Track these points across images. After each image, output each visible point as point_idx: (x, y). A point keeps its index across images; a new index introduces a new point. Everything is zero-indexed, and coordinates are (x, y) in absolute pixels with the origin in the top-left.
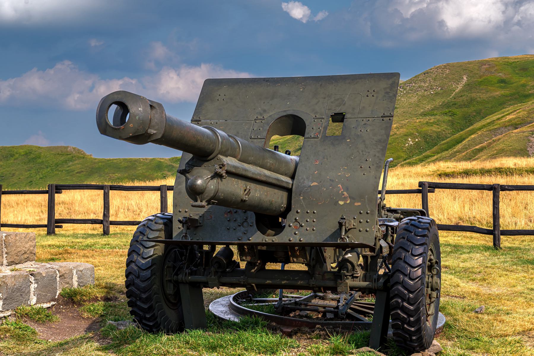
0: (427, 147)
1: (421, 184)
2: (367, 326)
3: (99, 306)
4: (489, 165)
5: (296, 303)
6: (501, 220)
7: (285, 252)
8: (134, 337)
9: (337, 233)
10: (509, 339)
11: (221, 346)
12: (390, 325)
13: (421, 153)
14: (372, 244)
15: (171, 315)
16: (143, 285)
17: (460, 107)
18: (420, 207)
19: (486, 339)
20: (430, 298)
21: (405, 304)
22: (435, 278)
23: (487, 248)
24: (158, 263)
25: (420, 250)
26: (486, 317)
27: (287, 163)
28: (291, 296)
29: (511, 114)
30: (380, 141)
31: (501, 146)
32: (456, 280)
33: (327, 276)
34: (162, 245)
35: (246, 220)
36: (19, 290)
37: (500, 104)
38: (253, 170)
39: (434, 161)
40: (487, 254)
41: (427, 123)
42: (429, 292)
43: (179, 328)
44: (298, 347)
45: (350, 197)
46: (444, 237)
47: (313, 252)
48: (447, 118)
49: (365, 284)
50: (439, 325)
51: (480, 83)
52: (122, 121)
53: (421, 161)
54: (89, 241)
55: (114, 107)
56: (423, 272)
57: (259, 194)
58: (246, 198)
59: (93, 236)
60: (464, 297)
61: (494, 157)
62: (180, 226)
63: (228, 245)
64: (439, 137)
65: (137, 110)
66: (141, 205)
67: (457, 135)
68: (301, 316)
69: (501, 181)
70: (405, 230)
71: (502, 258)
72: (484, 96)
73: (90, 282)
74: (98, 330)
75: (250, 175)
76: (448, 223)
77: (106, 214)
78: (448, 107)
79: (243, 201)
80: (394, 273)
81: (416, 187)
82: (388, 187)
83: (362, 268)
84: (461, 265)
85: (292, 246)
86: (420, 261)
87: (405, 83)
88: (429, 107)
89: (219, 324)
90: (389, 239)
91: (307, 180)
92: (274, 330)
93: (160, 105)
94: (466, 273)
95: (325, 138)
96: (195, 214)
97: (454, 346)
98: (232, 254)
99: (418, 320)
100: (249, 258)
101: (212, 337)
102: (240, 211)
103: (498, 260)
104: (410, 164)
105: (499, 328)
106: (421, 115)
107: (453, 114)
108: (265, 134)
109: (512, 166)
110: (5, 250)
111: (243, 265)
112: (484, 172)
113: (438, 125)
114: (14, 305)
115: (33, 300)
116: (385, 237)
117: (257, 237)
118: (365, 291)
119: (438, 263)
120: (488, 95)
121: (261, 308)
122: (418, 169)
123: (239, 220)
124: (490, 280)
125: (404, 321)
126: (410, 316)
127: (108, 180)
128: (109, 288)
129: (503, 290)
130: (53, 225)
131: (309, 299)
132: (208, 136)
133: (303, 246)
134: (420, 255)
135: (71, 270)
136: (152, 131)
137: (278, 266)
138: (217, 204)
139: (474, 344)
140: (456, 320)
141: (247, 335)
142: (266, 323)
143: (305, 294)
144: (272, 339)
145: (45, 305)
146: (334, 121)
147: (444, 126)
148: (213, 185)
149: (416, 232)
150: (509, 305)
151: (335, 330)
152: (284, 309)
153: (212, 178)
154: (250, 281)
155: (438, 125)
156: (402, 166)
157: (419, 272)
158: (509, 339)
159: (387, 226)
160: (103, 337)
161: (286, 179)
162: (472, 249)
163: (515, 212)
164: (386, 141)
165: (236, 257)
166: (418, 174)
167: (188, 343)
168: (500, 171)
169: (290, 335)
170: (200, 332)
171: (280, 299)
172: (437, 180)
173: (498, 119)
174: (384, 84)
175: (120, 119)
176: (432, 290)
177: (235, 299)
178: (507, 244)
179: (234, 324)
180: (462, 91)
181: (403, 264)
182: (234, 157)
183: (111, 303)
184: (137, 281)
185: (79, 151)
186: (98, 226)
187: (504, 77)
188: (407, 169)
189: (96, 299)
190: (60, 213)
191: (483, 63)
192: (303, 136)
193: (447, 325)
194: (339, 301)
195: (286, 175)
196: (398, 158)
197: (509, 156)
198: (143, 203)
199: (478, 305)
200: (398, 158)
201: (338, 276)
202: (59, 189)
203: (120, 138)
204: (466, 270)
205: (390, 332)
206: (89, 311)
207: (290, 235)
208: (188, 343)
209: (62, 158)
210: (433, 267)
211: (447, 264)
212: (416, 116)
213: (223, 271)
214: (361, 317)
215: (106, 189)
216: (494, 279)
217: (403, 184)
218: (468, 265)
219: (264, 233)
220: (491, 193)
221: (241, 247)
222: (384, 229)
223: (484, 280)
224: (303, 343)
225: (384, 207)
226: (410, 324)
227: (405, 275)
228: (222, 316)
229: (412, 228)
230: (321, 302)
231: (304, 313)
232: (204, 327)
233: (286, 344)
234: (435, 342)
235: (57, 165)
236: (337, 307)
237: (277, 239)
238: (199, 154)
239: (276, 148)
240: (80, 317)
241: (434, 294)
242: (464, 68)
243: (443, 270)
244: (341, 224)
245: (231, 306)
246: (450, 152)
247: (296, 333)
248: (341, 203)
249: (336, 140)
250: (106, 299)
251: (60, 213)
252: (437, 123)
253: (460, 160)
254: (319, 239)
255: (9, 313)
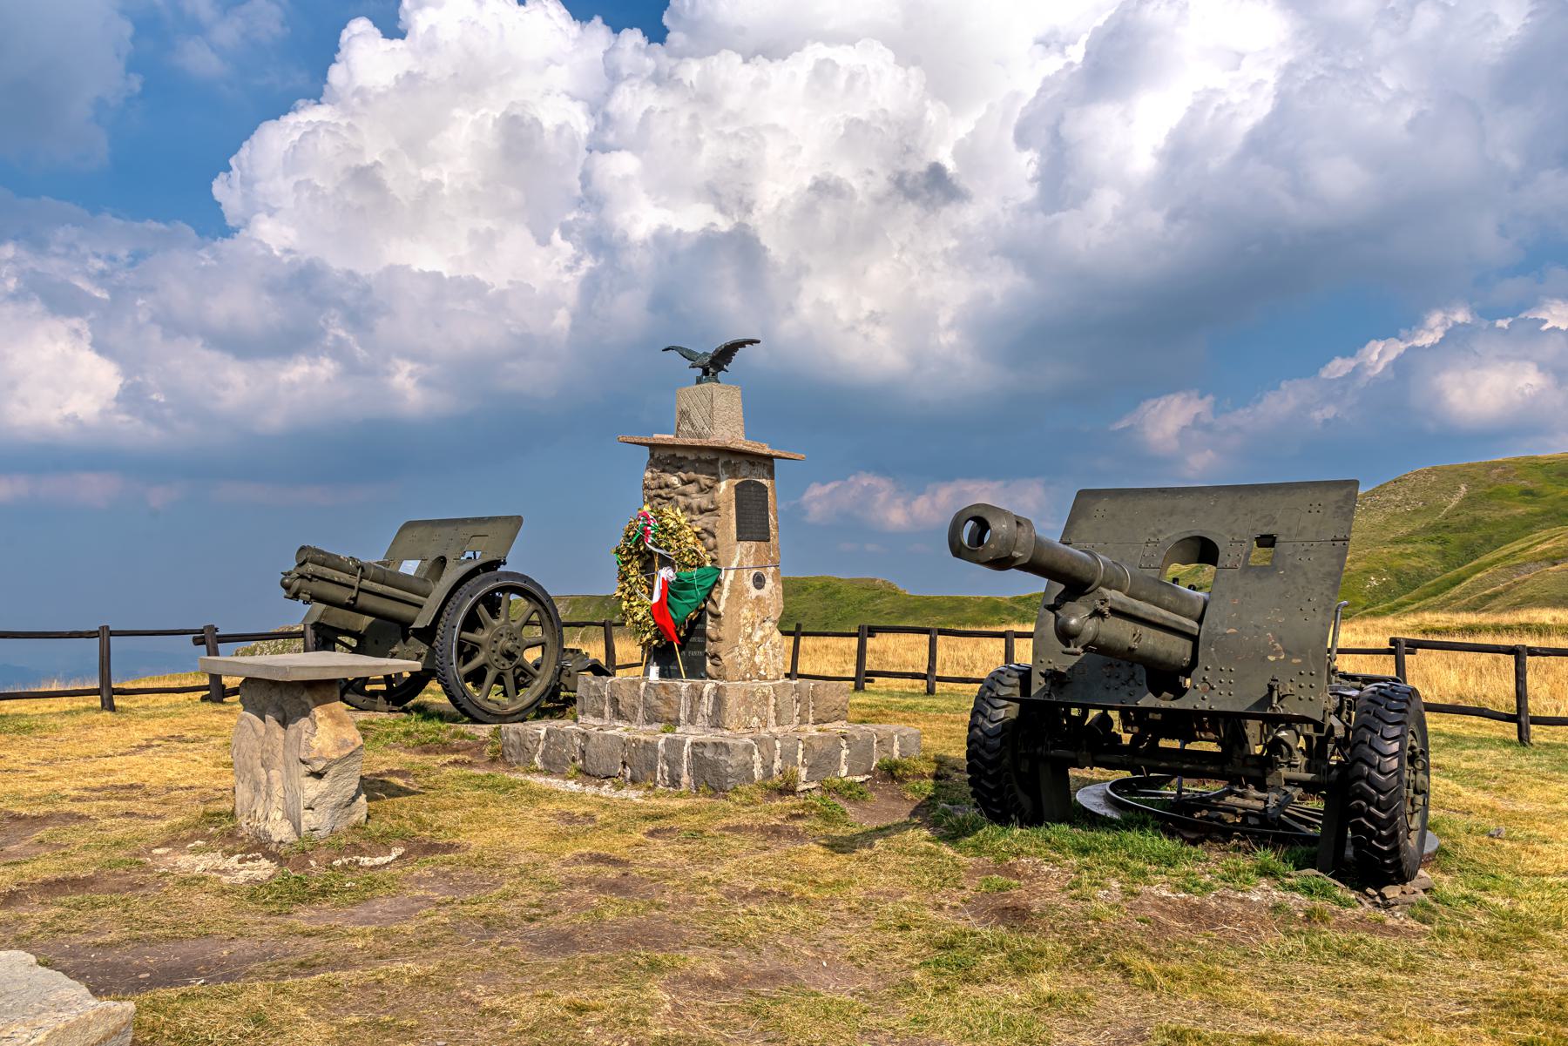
0: (1403, 589)
1: (1393, 641)
2: (1311, 840)
3: (928, 786)
4: (1506, 619)
5: (1202, 799)
6: (1530, 703)
7: (1185, 723)
8: (975, 828)
9: (1266, 700)
10: (1550, 880)
11: (1096, 849)
12: (1349, 843)
13: (1391, 598)
14: (1319, 719)
15: (1025, 800)
16: (989, 758)
17: (1457, 530)
18: (1393, 674)
19: (1509, 877)
20: (1413, 805)
21: (1373, 809)
22: (1420, 776)
23: (1507, 743)
24: (1009, 727)
25: (1396, 731)
26: (1507, 844)
27: (1192, 601)
28: (1192, 788)
29: (1544, 542)
30: (1329, 574)
31: (1529, 591)
32: (1454, 786)
33: (1249, 762)
34: (1017, 705)
35: (1132, 677)
36: (827, 755)
37: (1526, 527)
38: (1145, 609)
39: (1415, 611)
40: (1508, 751)
41: (1401, 554)
42: (1411, 794)
43: (1034, 819)
44: (1207, 860)
45: (1286, 651)
46: (1433, 721)
47: (1229, 725)
48: (1434, 547)
49: (1309, 776)
50: (1428, 849)
51: (1489, 496)
52: (980, 541)
53: (1392, 610)
54: (909, 701)
55: (971, 523)
56: (1401, 764)
57: (1153, 642)
58: (1135, 645)
59: (913, 695)
60: (1470, 813)
61: (1516, 607)
62: (1042, 680)
63: (1106, 708)
64: (1421, 576)
65: (999, 527)
66: (985, 657)
67: (1452, 573)
68: (1211, 819)
69: (1530, 642)
70: (1370, 700)
71: (1534, 760)
72: (1497, 515)
73: (915, 754)
74: (926, 812)
75: (1141, 614)
76: (1440, 702)
77: (932, 667)
78: (1437, 532)
79: (1131, 650)
80: (1354, 762)
81: (1386, 645)
82: (1341, 645)
83: (1304, 753)
84: (1464, 765)
85: (1197, 714)
86: (1395, 747)
87: (1364, 496)
88: (1403, 530)
89: (1090, 820)
90: (1344, 716)
91: (1220, 624)
92: (1171, 835)
93: (1028, 522)
94: (1476, 779)
95: (1247, 568)
96: (1063, 664)
97: (1453, 882)
98: (1110, 722)
99: (1394, 835)
100: (1136, 729)
101: (1083, 836)
102: (1124, 664)
103: (1526, 760)
104: (1375, 615)
105: (1530, 862)
106: (1391, 542)
107: (1445, 542)
108: (1160, 562)
109: (1549, 622)
110: (812, 704)
111: (1126, 739)
112: (1498, 629)
113: (1422, 557)
114: (821, 775)
115: (844, 771)
116: (1338, 712)
117: (1148, 701)
118: (1309, 788)
119: (1425, 753)
120: (1504, 513)
121: (1152, 803)
122: (1389, 621)
123: (1124, 676)
124: (1513, 790)
125: (1370, 834)
126: (1380, 828)
127: (938, 621)
128: (941, 761)
129: (1536, 807)
130: (863, 677)
131: (1221, 796)
132: (1086, 563)
133: (1215, 717)
134: (1395, 738)
135: (892, 736)
136: (1017, 554)
137: (1176, 744)
138: (1097, 652)
139: (1487, 882)
140: (1456, 845)
141: (1133, 836)
142: (1157, 823)
143: (1213, 787)
144: (1167, 844)
145: (859, 779)
146: (1259, 546)
147: (1430, 560)
148: (1091, 626)
149: (1392, 704)
150: (1549, 830)
151: (1261, 840)
152: (1183, 806)
153: (1091, 616)
154: (1137, 761)
155: (1422, 557)
156: (1362, 617)
157: (1395, 763)
158: (1550, 880)
159: (1342, 696)
160: (934, 824)
161: (1191, 624)
162: (1482, 742)
163: (1550, 688)
164: (1339, 574)
165: (1117, 727)
166: (1389, 629)
167: (1048, 841)
168: (1527, 628)
169: (1194, 843)
170: (1065, 828)
171: (1179, 792)
172: (1419, 637)
173: (1523, 550)
174: (1335, 496)
175: (974, 538)
176: (1416, 792)
177: (1111, 787)
178: (1543, 739)
179: (1111, 821)
180: (1457, 507)
181: (1368, 750)
182: (1120, 590)
183: (942, 782)
184: (982, 752)
185: (869, 586)
186: (918, 682)
187: (1530, 486)
188: (1368, 622)
189: (922, 776)
190: (871, 663)
191: (1493, 466)
192: (1215, 564)
193: (1441, 851)
194: (1266, 802)
195: (1190, 617)
196: (1355, 604)
197: (1542, 606)
198: (977, 655)
199: (1493, 826)
200: (1355, 604)
201: (1266, 764)
202: (872, 631)
203: (978, 562)
204: (1471, 773)
205: (1349, 852)
206: (914, 790)
207: (1197, 697)
208: (1048, 841)
209: (868, 594)
210: (1416, 758)
211: (1439, 761)
212: (1382, 543)
213: (1100, 747)
214: (1303, 827)
215: (932, 633)
216: (1520, 789)
217: (1363, 643)
218: (1474, 765)
219: (1157, 695)
220: (1512, 658)
221: (1124, 713)
222: (1336, 701)
223: (1504, 789)
224: (1214, 855)
225: (1334, 671)
226: (1381, 840)
227: (1371, 766)
228: (1095, 809)
229: (1381, 699)
230: (1239, 801)
231: (1214, 814)
232: (1072, 823)
233: (1189, 854)
234: (1421, 872)
235: (860, 602)
236: (1265, 809)
237: (1175, 705)
238: (1074, 586)
239: (1175, 580)
240: (902, 798)
241: (1419, 799)
242: (1462, 474)
243: (1432, 770)
244: (1271, 689)
245: (1107, 797)
246: (1441, 597)
247: (1202, 841)
248: (1272, 658)
249: (1262, 572)
250: (937, 777)
251: (871, 663)
252: (1418, 555)
253: (1457, 611)
254: (1240, 708)
255: (814, 785)
